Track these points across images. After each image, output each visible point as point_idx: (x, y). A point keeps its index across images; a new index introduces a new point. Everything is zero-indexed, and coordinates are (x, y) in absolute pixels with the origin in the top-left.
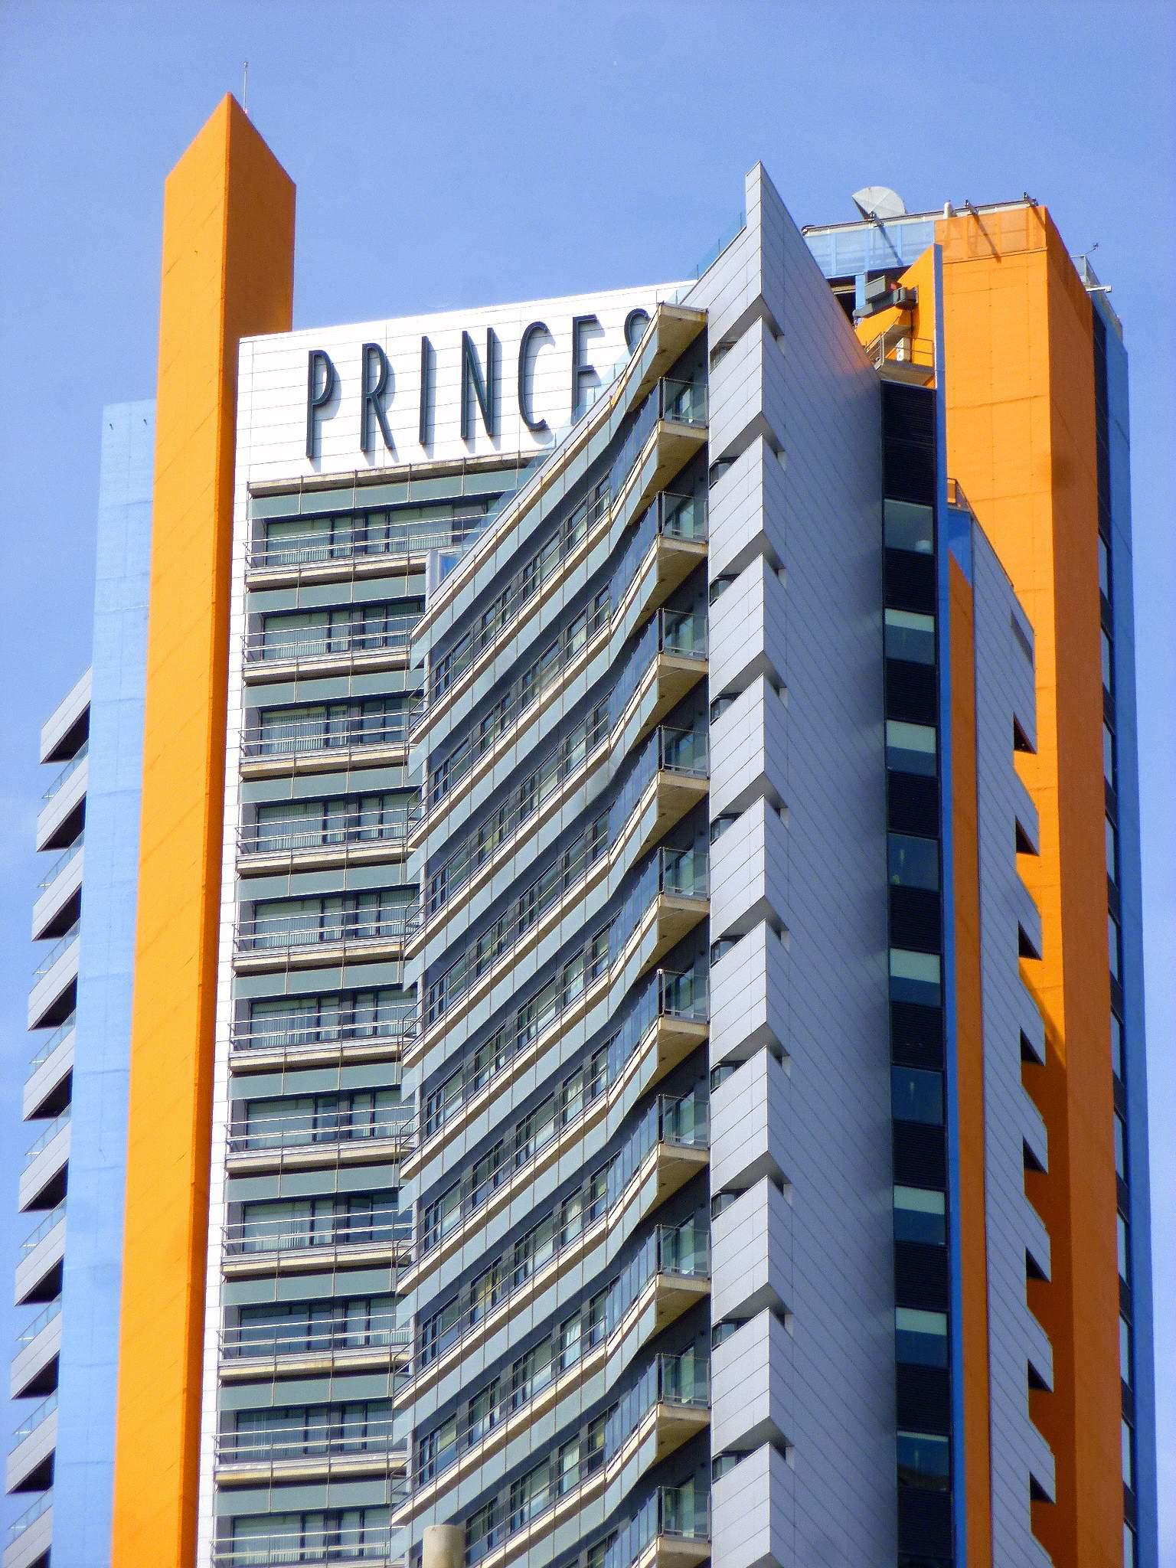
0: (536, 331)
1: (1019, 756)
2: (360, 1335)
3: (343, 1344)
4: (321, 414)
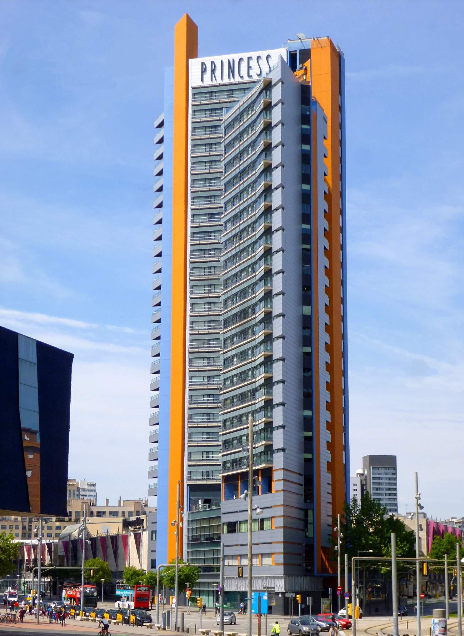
0: (241, 60)
1: (324, 140)
2: (214, 149)
3: (211, 239)
4: (204, 73)
